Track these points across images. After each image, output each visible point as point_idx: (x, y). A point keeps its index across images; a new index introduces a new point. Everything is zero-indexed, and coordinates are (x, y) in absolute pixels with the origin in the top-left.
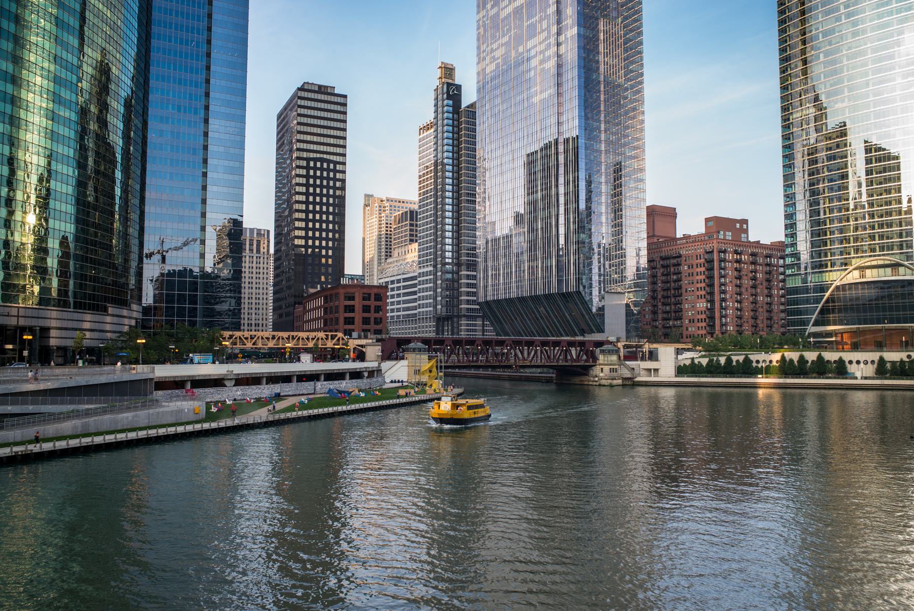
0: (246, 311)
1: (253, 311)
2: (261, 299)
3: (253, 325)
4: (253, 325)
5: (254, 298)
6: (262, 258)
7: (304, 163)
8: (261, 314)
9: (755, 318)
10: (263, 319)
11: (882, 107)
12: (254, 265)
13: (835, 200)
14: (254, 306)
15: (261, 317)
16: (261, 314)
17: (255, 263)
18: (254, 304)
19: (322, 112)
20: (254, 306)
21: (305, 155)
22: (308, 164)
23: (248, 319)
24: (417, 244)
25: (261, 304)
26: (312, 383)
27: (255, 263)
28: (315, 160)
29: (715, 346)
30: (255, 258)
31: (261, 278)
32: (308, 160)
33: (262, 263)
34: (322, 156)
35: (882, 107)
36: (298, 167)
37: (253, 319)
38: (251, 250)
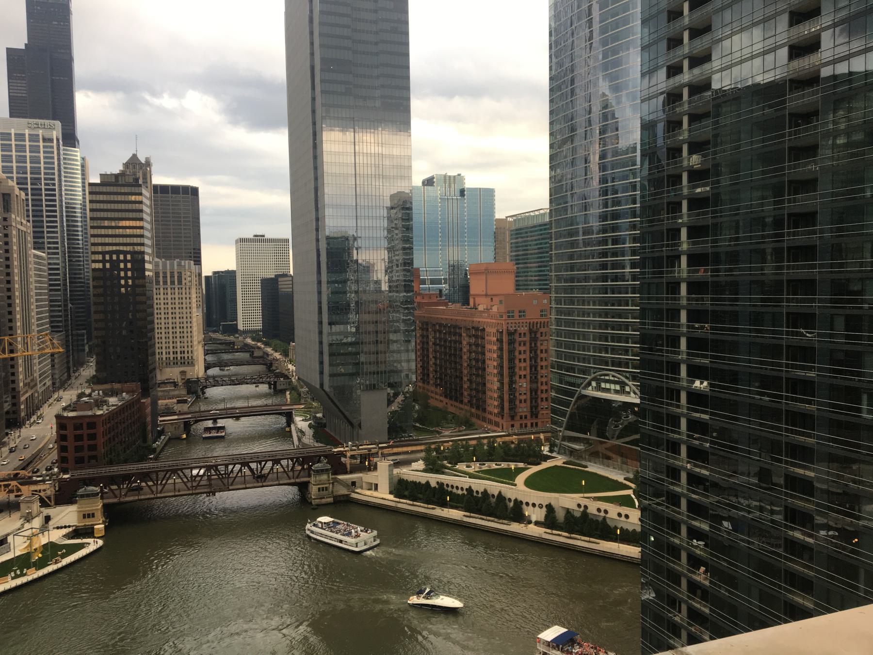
1: (178, 340)
2: (185, 327)
3: (179, 353)
4: (179, 353)
5: (178, 327)
6: (184, 289)
7: (100, 257)
8: (186, 342)
10: (188, 347)
11: (617, 208)
12: (177, 296)
14: (178, 335)
16: (186, 342)
17: (177, 293)
18: (178, 333)
19: (116, 205)
20: (178, 335)
21: (100, 249)
22: (104, 257)
23: (173, 347)
25: (185, 332)
27: (177, 293)
28: (111, 253)
29: (33, 534)
30: (176, 289)
32: (103, 253)
33: (184, 293)
34: (118, 248)
35: (617, 208)
36: (94, 261)
37: (179, 347)
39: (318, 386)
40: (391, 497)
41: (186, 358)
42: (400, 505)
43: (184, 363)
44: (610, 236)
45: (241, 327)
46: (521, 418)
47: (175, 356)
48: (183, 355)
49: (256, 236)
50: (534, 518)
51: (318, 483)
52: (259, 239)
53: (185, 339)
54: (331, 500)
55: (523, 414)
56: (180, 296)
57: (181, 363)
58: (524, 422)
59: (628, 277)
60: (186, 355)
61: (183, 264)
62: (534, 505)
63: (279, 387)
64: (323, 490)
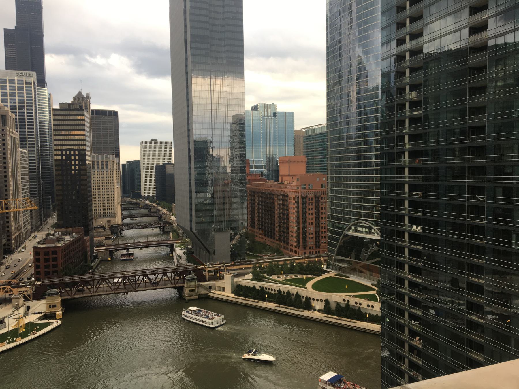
0: (459, 44)
1: (106, 202)
2: (110, 194)
3: (106, 209)
4: (106, 209)
5: (106, 194)
6: (109, 172)
7: (60, 153)
8: (110, 203)
10: (112, 206)
11: (367, 124)
12: (105, 176)
13: (352, 187)
14: (106, 199)
16: (110, 203)
17: (105, 174)
18: (106, 198)
19: (69, 122)
20: (106, 199)
21: (59, 148)
22: (62, 153)
23: (103, 206)
25: (110, 197)
27: (105, 174)
28: (66, 150)
30: (105, 172)
32: (61, 150)
33: (109, 174)
34: (70, 147)
35: (367, 124)
36: (56, 155)
37: (106, 206)
39: (189, 229)
40: (233, 295)
41: (111, 213)
42: (238, 300)
43: (110, 215)
44: (362, 140)
45: (143, 194)
46: (310, 248)
47: (104, 211)
48: (109, 211)
49: (152, 140)
50: (317, 308)
51: (189, 287)
52: (154, 142)
55: (311, 246)
56: (107, 176)
57: (108, 216)
59: (373, 164)
60: (111, 211)
61: (109, 157)
62: (317, 300)
63: (166, 230)
64: (192, 291)
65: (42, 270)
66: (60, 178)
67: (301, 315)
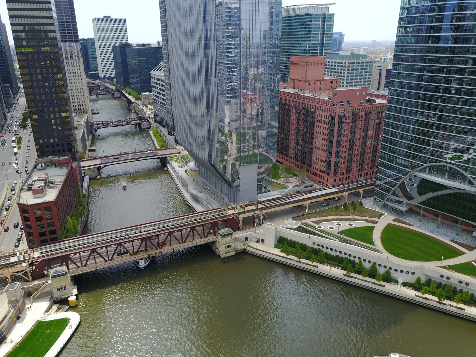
1: (75, 97)
3: (77, 106)
4: (77, 106)
6: (75, 63)
8: (80, 99)
9: (351, 148)
10: (82, 102)
15: (81, 100)
17: (71, 66)
24: (464, 159)
26: (77, 140)
27: (71, 66)
30: (70, 63)
31: (77, 76)
33: (75, 66)
37: (76, 102)
38: (67, 58)
39: (207, 160)
40: (277, 251)
41: (82, 109)
43: (81, 112)
44: (471, 58)
45: (101, 75)
47: (75, 108)
48: (79, 107)
49: (105, 17)
50: (400, 280)
51: (224, 243)
52: (107, 19)
53: (80, 97)
54: (233, 253)
55: (342, 172)
56: (73, 68)
57: (79, 112)
58: (341, 177)
60: (82, 107)
61: (72, 45)
62: (402, 271)
63: (143, 127)
64: (228, 247)
65: (36, 229)
66: (31, 91)
67: (383, 292)
